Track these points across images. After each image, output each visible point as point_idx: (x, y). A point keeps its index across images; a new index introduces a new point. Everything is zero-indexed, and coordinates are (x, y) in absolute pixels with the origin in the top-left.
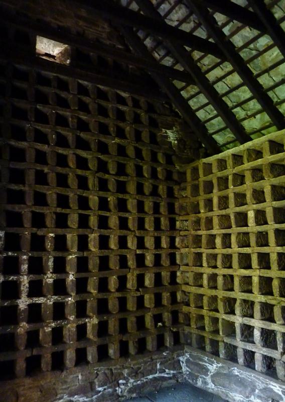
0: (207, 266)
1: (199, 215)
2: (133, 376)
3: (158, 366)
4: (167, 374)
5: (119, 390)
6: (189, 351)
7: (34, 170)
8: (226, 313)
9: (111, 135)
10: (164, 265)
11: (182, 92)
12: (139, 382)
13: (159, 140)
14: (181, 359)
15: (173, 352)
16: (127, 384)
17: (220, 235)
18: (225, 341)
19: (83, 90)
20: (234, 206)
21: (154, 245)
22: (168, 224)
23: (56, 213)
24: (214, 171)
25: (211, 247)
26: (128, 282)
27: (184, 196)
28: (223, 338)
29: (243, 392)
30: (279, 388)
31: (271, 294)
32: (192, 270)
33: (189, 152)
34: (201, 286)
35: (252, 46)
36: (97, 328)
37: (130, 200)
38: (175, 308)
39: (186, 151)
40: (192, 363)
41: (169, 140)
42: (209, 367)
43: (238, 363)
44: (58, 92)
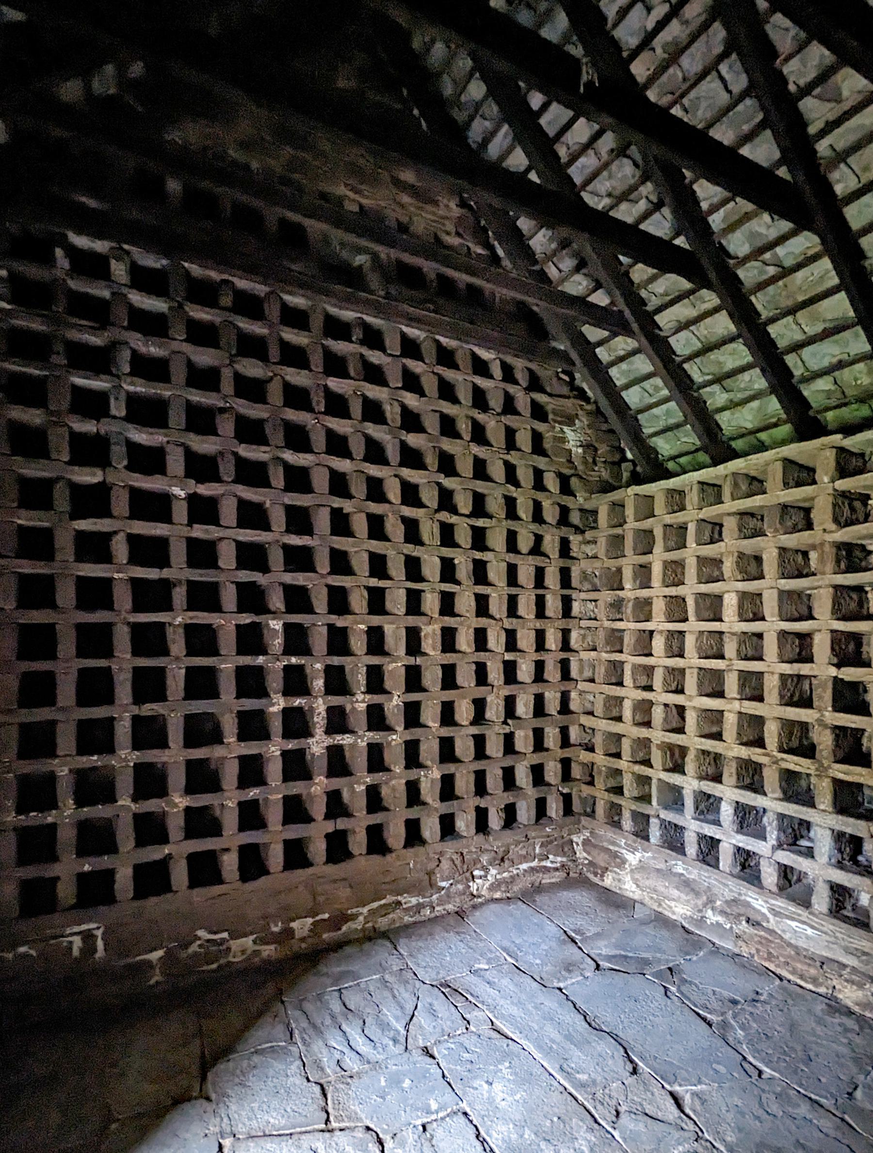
0: (632, 685)
1: (620, 593)
3: (537, 851)
5: (474, 887)
7: (329, 509)
8: (665, 770)
9: (461, 438)
11: (598, 350)
12: (505, 875)
16: (486, 876)
17: (661, 632)
18: (662, 816)
19: (411, 348)
20: (696, 581)
22: (560, 607)
23: (368, 589)
25: (641, 653)
26: (488, 709)
27: (590, 555)
28: (657, 810)
30: (763, 903)
34: (619, 719)
35: (767, 256)
36: (438, 786)
38: (567, 753)
39: (596, 468)
41: (568, 446)
42: (626, 856)
44: (365, 351)
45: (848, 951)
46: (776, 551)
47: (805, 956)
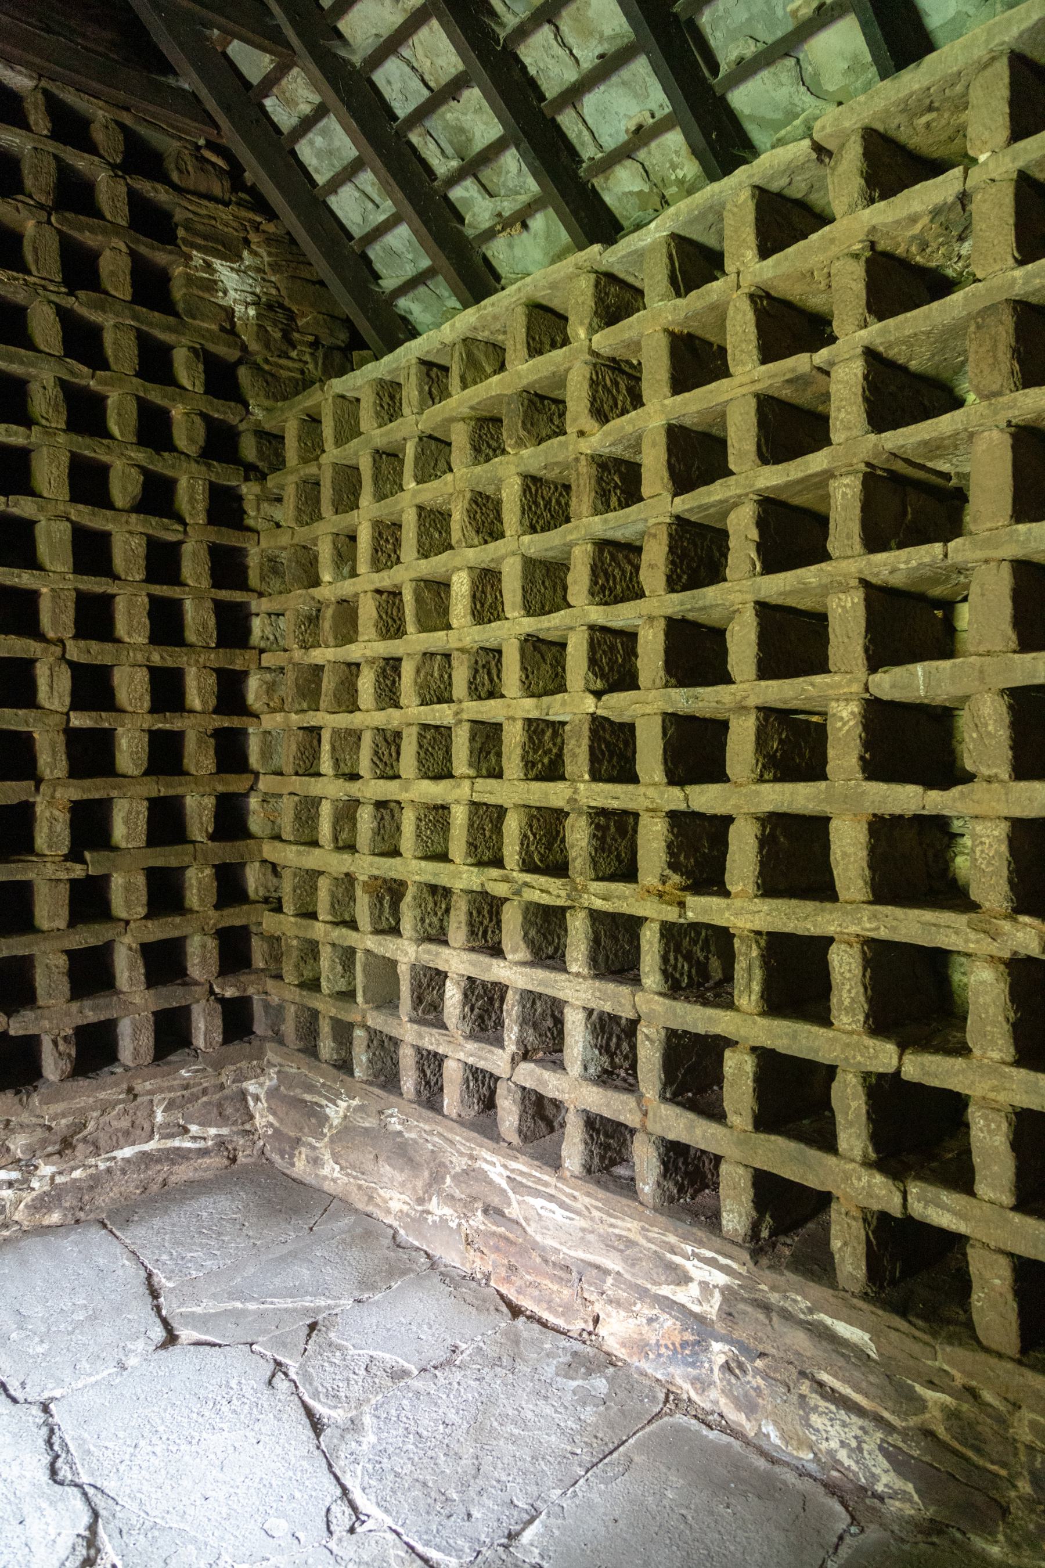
2: (49, 1155)
3: (159, 1117)
4: (194, 1138)
6: (276, 1060)
10: (193, 771)
12: (77, 1174)
13: (178, 292)
14: (251, 1087)
15: (218, 1066)
17: (371, 662)
21: (148, 698)
24: (364, 426)
29: (409, 1185)
31: (498, 862)
32: (291, 789)
33: (307, 358)
37: (43, 523)
38: (234, 917)
39: (294, 354)
40: (284, 1099)
41: (220, 299)
43: (401, 1094)
45: (609, 1244)
46: (518, 480)
47: (554, 1264)
